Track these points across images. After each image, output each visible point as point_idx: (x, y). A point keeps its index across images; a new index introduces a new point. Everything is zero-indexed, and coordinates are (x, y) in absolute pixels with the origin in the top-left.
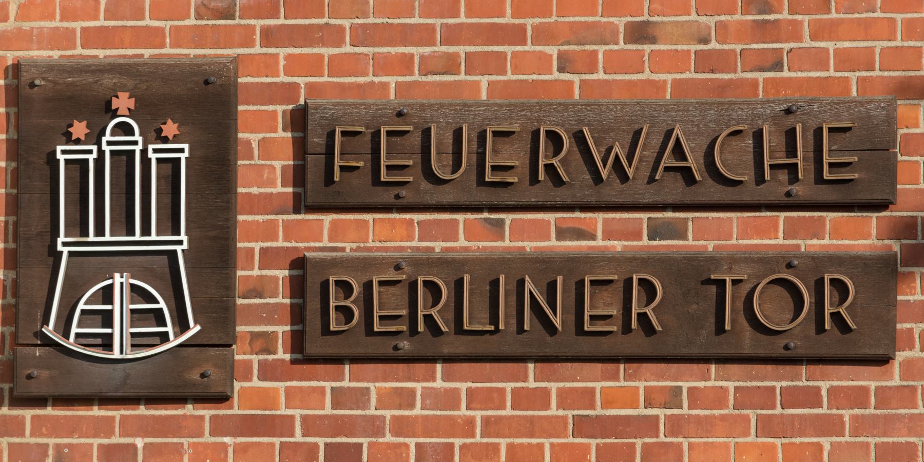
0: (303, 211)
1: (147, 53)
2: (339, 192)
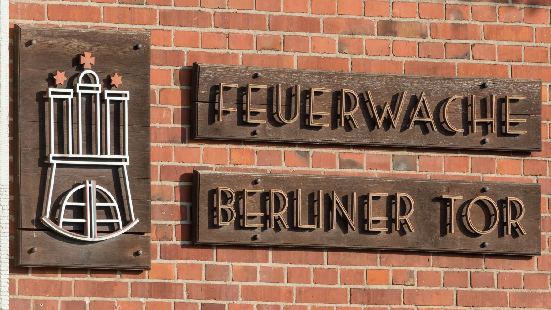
0: (187, 141)
1: (89, 24)
2: (217, 129)
